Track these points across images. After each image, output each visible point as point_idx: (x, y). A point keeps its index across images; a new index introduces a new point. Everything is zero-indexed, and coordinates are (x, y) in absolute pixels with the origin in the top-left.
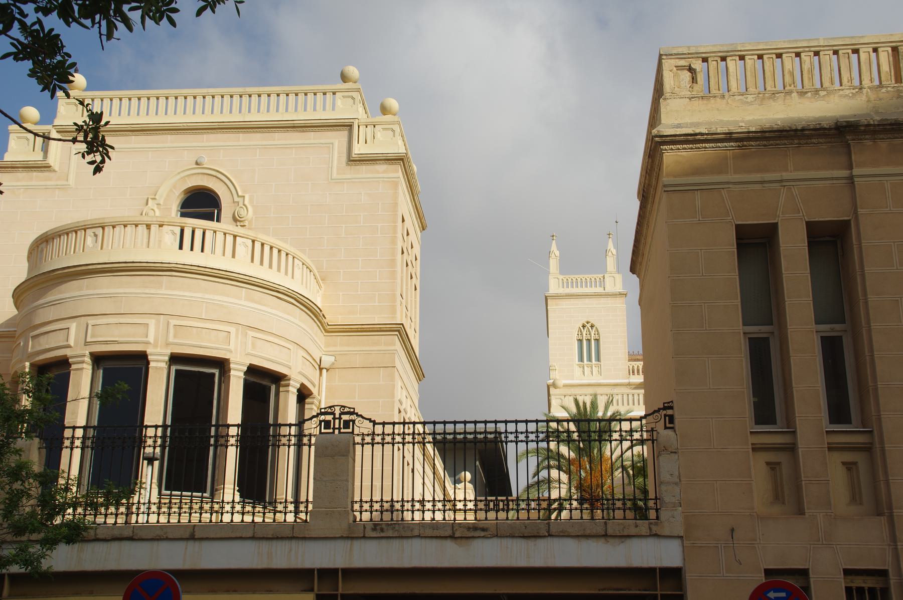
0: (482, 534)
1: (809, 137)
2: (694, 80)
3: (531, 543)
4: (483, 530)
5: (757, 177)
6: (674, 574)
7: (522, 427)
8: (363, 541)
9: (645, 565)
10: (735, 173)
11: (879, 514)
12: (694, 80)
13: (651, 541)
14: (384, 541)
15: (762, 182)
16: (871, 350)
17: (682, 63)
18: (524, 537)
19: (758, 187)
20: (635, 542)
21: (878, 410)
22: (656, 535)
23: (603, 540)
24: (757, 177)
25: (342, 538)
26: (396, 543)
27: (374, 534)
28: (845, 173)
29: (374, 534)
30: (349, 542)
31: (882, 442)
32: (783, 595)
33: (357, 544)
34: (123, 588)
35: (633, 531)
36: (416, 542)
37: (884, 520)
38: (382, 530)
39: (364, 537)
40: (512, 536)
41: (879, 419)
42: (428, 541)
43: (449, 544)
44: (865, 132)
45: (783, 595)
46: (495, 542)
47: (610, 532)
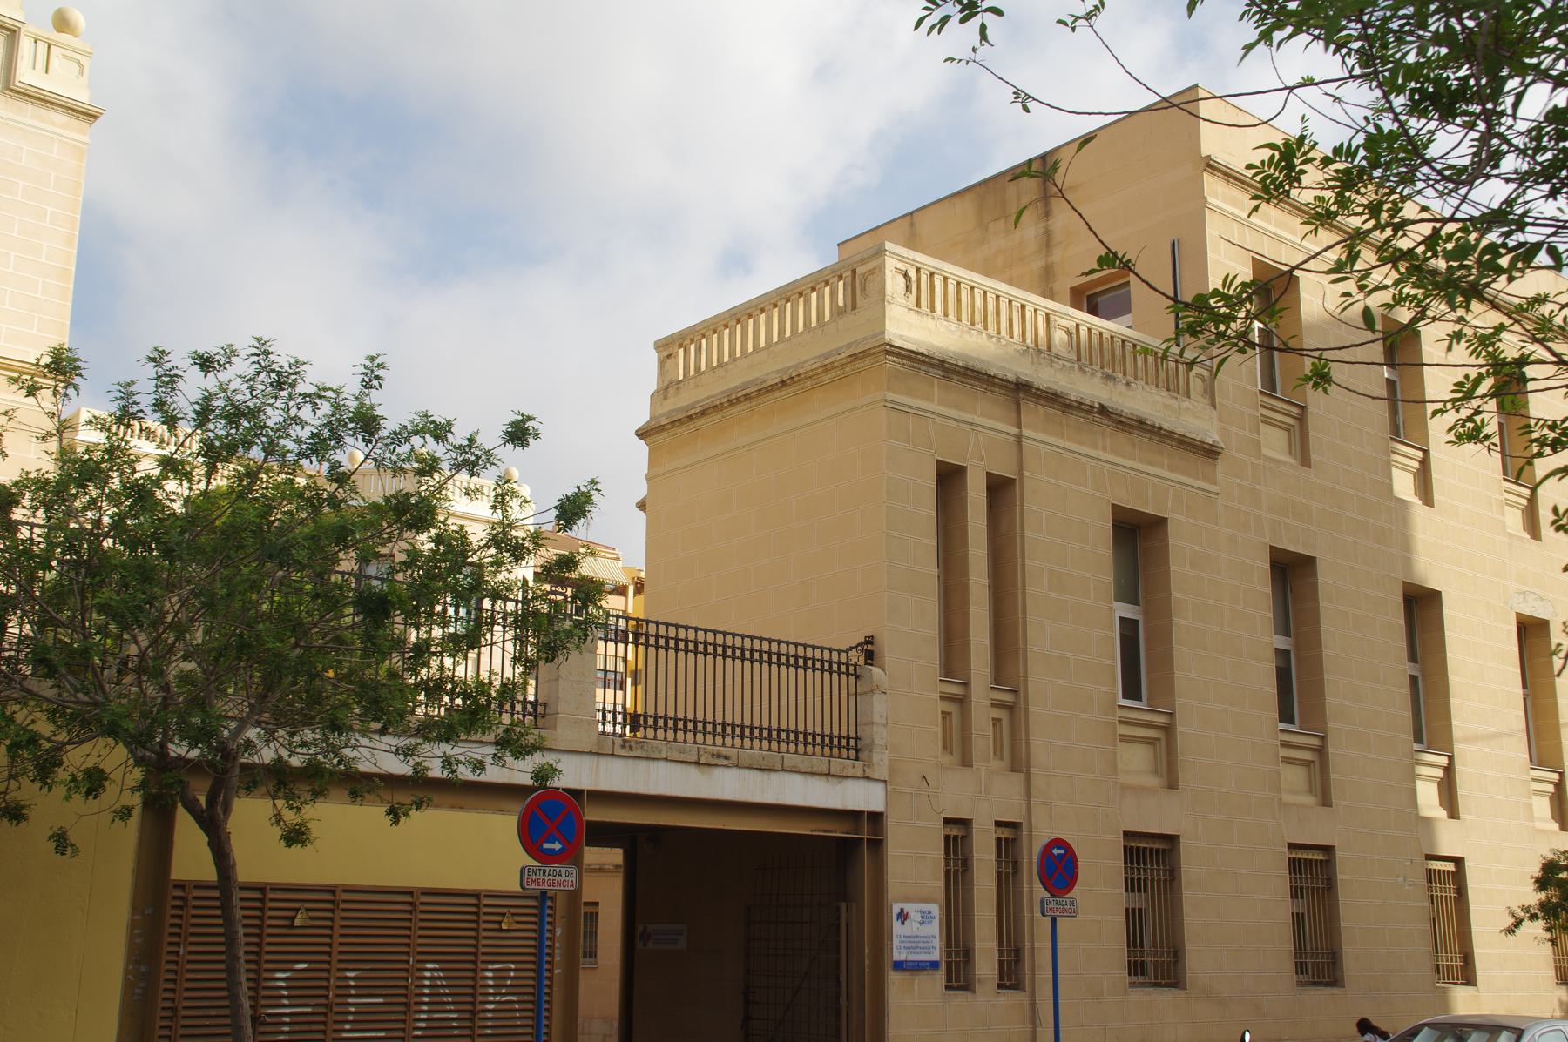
0: (725, 762)
1: (994, 385)
2: (82, 73)
3: (765, 775)
4: (726, 758)
5: (954, 413)
6: (876, 818)
7: (662, 631)
8: (609, 759)
9: (856, 808)
10: (982, 415)
11: (1015, 768)
12: (82, 73)
13: (862, 783)
14: (631, 761)
15: (958, 421)
16: (1025, 614)
17: (901, 266)
18: (760, 769)
19: (954, 424)
20: (850, 782)
21: (1026, 672)
22: (868, 778)
23: (824, 779)
24: (954, 413)
25: (590, 753)
26: (643, 763)
27: (623, 752)
28: (1015, 431)
29: (623, 752)
30: (595, 759)
31: (1026, 703)
32: (546, 846)
33: (603, 761)
34: (518, 807)
35: (850, 772)
36: (662, 764)
37: (1018, 779)
38: (631, 748)
39: (613, 755)
40: (750, 768)
41: (1026, 681)
42: (673, 765)
43: (693, 769)
44: (1034, 395)
45: (546, 846)
46: (735, 771)
47: (786, 766)
